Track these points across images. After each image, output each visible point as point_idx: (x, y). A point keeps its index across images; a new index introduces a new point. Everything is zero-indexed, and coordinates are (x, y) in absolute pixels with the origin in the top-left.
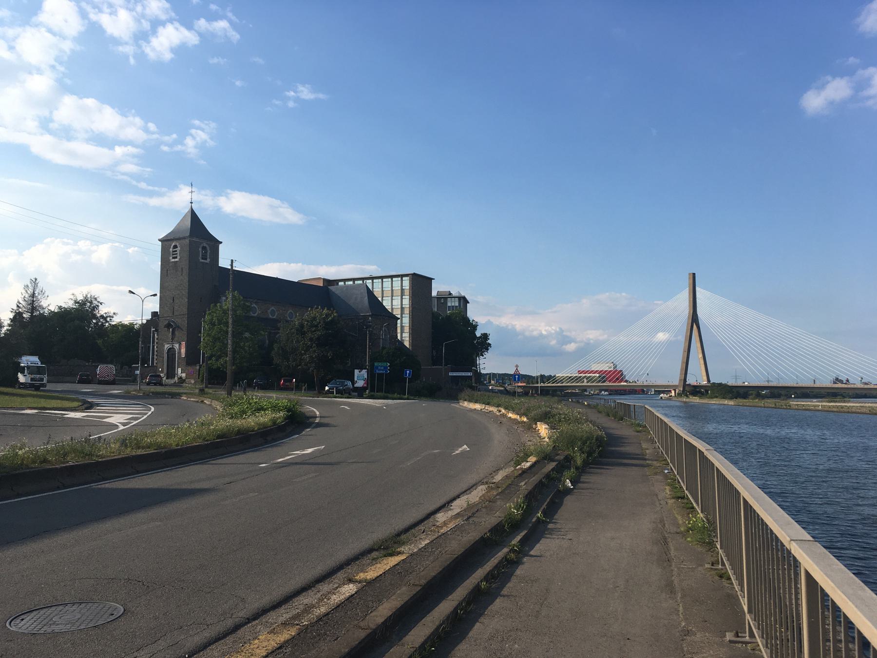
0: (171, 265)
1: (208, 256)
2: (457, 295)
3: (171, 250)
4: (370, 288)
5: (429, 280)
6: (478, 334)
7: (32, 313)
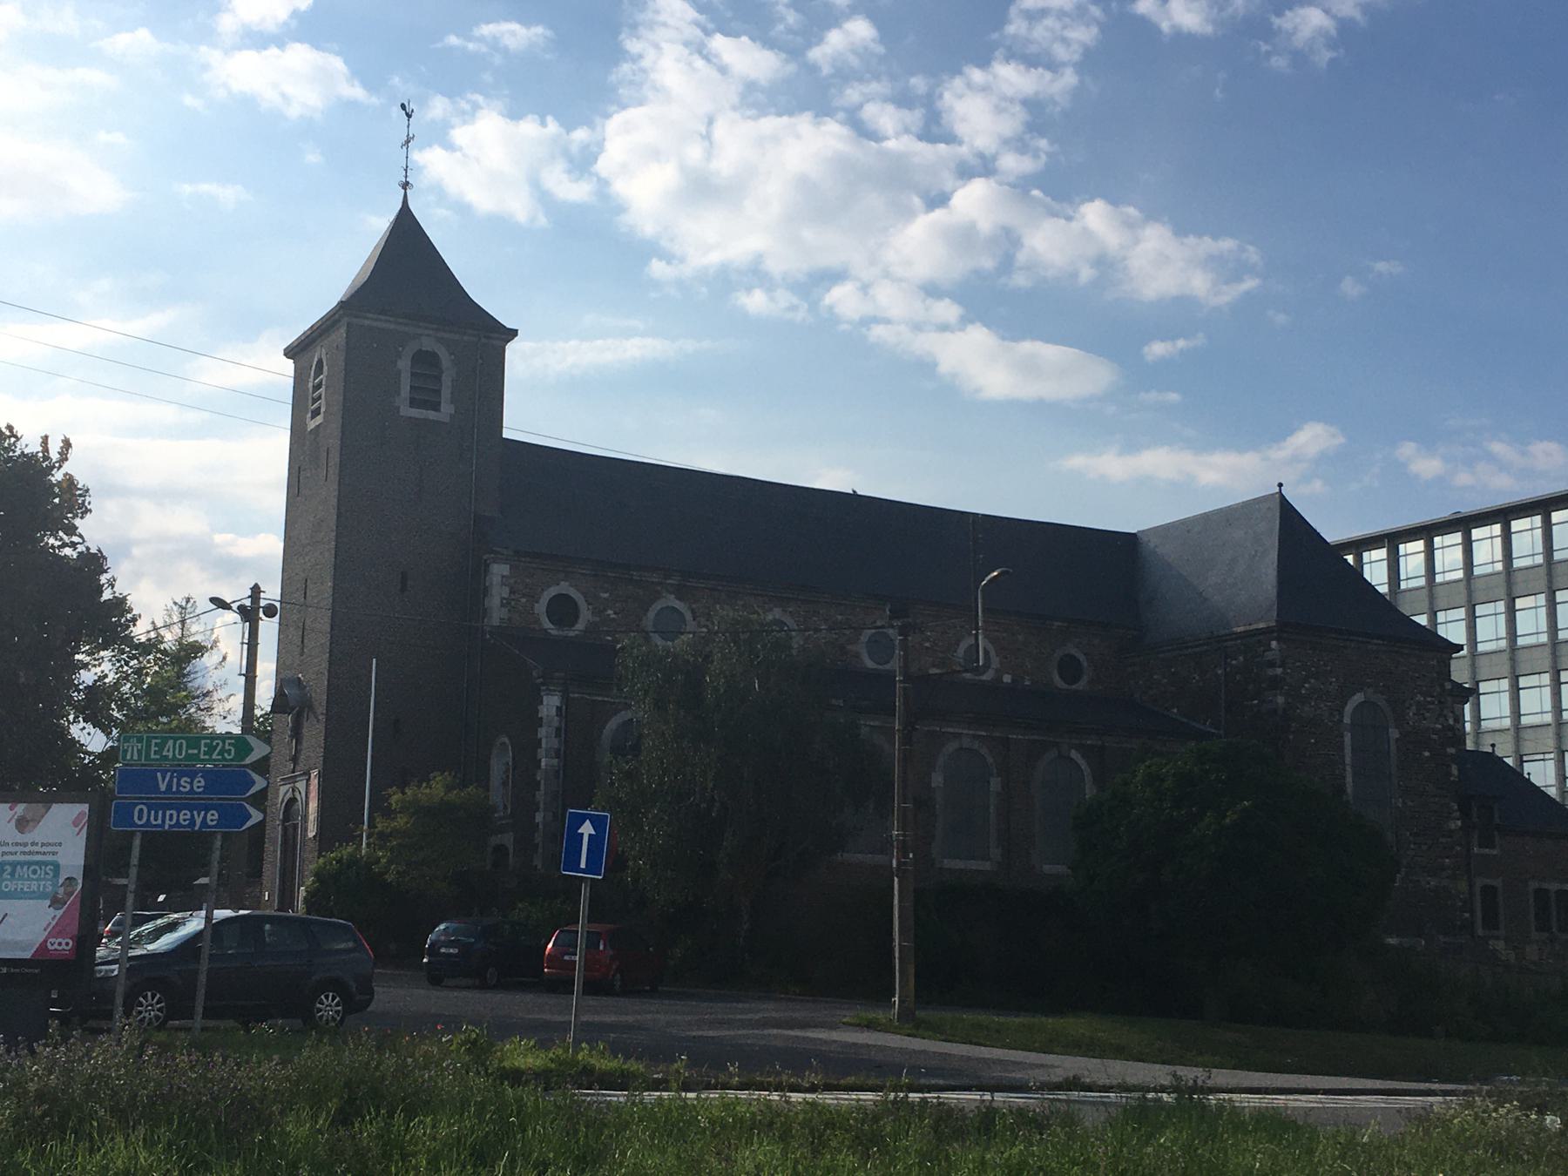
1: (446, 393)
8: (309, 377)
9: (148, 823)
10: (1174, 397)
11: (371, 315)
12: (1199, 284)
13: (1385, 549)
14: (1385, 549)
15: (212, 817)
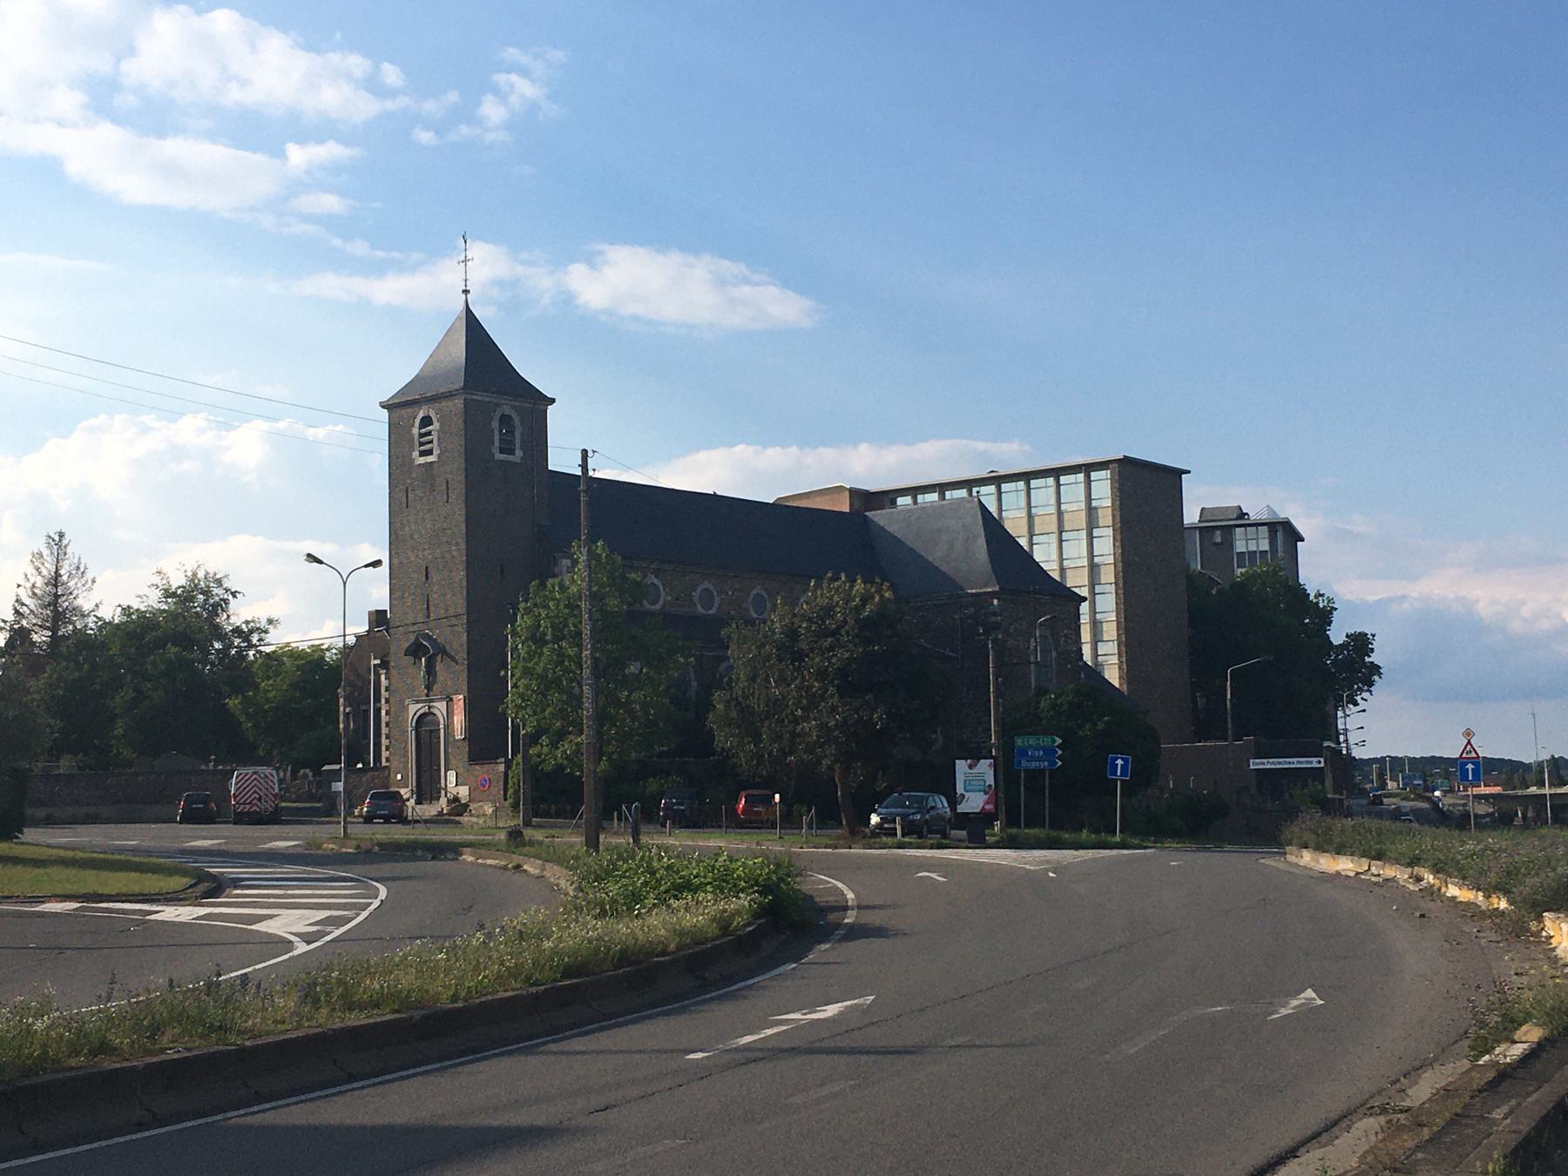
1: (518, 445)
3: (415, 431)
4: (993, 509)
6: (1337, 635)
7: (54, 630)
8: (413, 426)
13: (937, 494)
14: (937, 494)
15: (1046, 764)
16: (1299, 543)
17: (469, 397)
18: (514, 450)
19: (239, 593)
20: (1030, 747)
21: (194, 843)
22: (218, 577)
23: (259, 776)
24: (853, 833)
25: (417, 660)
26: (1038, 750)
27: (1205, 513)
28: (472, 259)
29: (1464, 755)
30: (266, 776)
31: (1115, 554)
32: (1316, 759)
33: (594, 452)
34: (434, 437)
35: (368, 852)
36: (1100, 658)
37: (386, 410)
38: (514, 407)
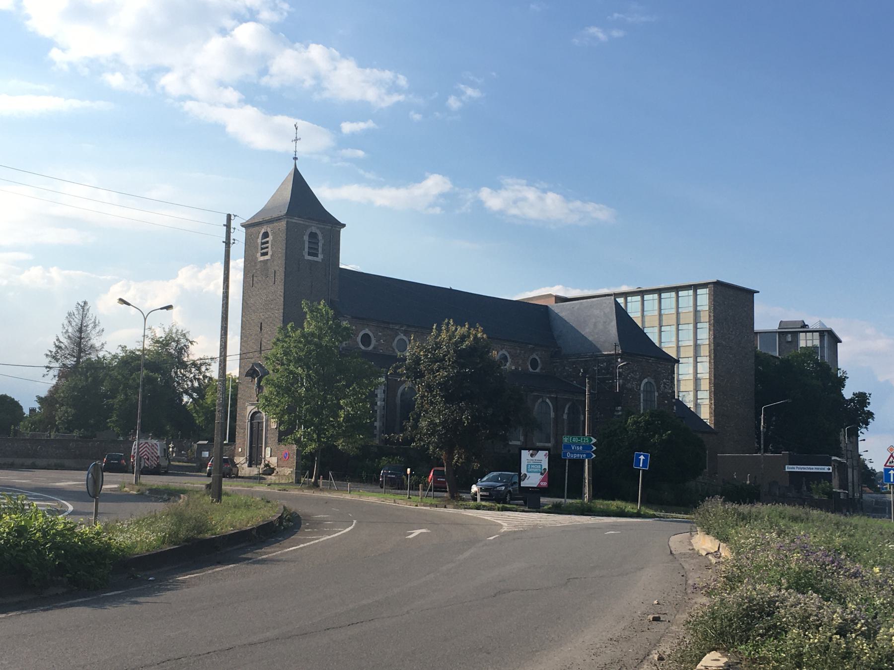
0: (258, 267)
1: (320, 250)
2: (818, 327)
3: (259, 241)
4: (623, 305)
5: (749, 294)
6: (848, 393)
7: (79, 357)
8: (258, 238)
9: (570, 457)
10: (360, 153)
11: (296, 218)
12: (371, 94)
15: (584, 455)
16: (838, 344)
17: (290, 220)
18: (318, 254)
19: (195, 342)
20: (574, 443)
21: (57, 484)
22: (184, 332)
23: (149, 445)
24: (453, 497)
25: (253, 379)
26: (579, 446)
27: (782, 324)
28: (300, 139)
29: (888, 464)
30: (153, 445)
31: (709, 339)
32: (828, 467)
33: (235, 216)
34: (269, 245)
35: (142, 494)
36: (699, 401)
37: (244, 228)
38: (318, 228)
